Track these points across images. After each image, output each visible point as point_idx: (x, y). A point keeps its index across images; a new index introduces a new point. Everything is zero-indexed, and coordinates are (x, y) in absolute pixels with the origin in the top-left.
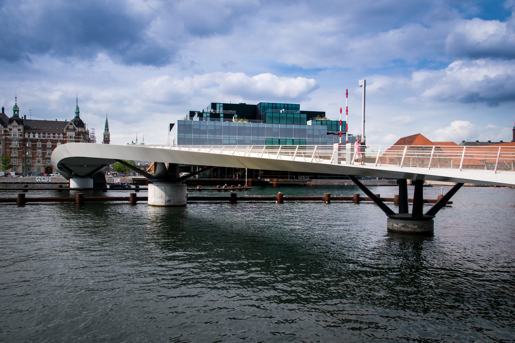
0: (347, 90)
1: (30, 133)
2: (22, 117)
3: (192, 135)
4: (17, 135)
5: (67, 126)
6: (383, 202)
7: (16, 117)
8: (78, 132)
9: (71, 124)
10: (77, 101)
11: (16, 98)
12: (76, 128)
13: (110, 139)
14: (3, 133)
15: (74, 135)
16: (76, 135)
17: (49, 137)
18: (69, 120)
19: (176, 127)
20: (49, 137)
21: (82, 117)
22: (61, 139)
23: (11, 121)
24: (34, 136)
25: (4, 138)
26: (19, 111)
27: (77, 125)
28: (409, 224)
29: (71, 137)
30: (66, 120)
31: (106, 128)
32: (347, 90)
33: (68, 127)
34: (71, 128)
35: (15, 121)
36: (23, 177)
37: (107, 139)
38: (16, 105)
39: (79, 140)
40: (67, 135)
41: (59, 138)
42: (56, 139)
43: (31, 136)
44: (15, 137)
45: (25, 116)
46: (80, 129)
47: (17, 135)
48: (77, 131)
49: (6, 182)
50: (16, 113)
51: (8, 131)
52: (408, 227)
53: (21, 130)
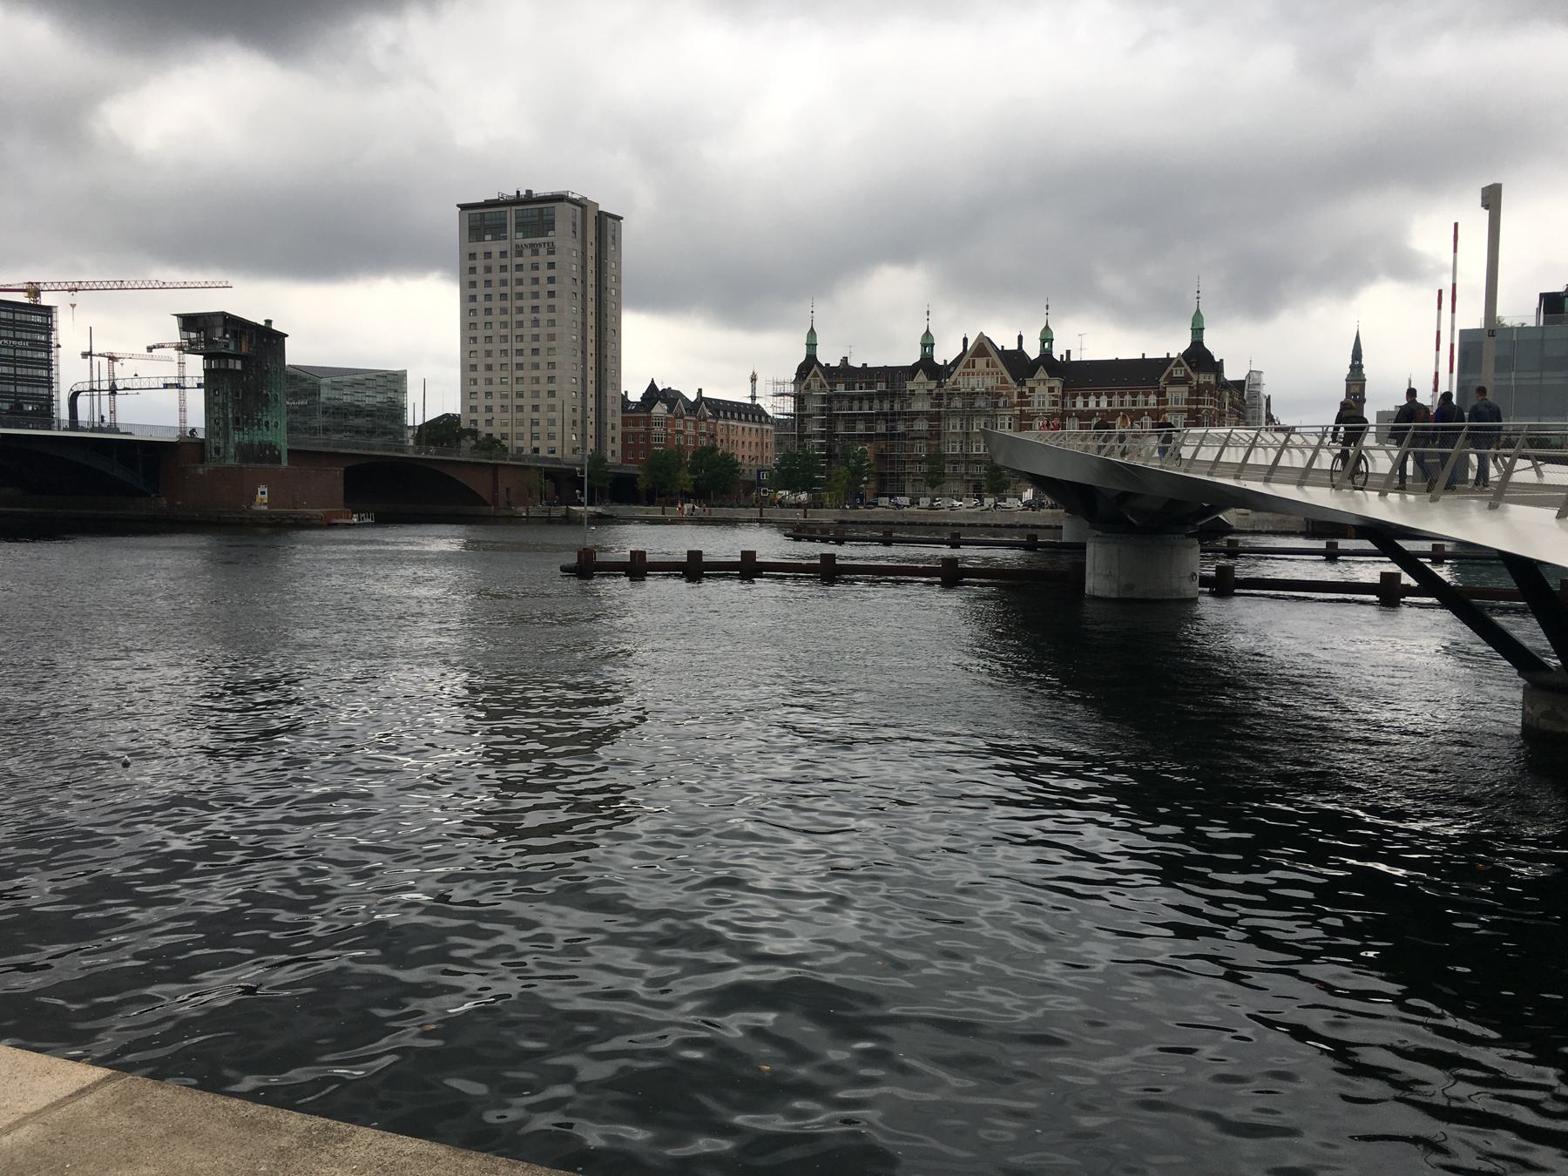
0: (1456, 225)
2: (1062, 356)
4: (1047, 403)
5: (1185, 365)
6: (1400, 543)
7: (1046, 355)
8: (1198, 385)
9: (1179, 364)
11: (928, 312)
12: (1192, 374)
13: (1366, 396)
14: (1015, 400)
15: (1186, 395)
16: (1191, 394)
17: (1134, 403)
18: (1173, 355)
20: (1122, 405)
22: (1152, 407)
23: (1035, 365)
24: (1086, 404)
25: (1018, 412)
26: (933, 344)
27: (1194, 365)
30: (1143, 355)
32: (1456, 225)
33: (1171, 372)
35: (1042, 367)
37: (1355, 396)
41: (1146, 404)
42: (1140, 407)
43: (1080, 405)
44: (1041, 407)
45: (1068, 352)
46: (1202, 375)
47: (1047, 403)
49: (989, 522)
53: (1056, 390)
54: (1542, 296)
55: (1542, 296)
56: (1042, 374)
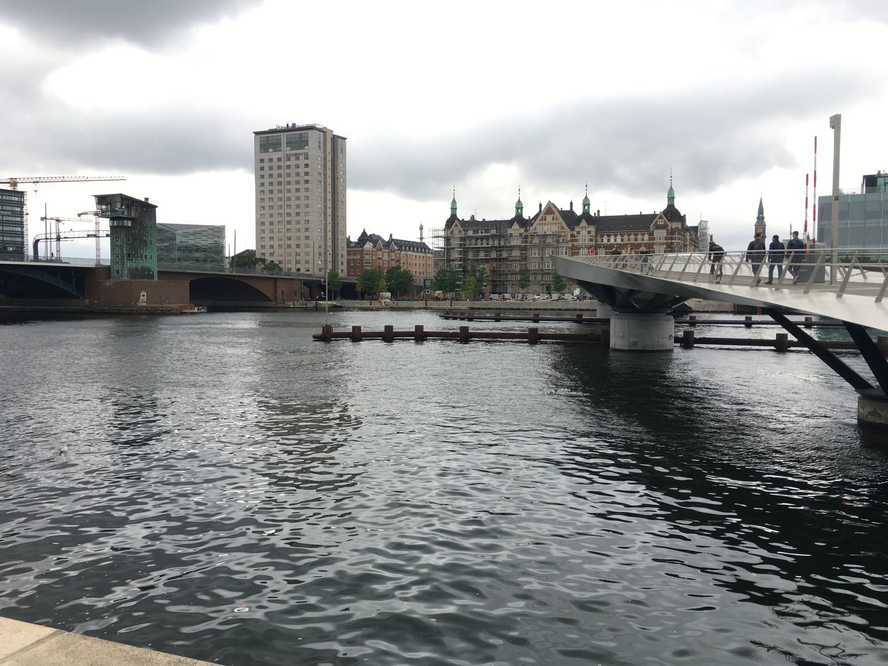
0: (816, 138)
1: (617, 235)
2: (595, 214)
3: (849, 223)
4: (587, 240)
7: (586, 214)
8: (672, 229)
9: (661, 217)
10: (671, 180)
11: (519, 190)
12: (668, 223)
14: (569, 238)
15: (665, 235)
18: (658, 212)
19: (263, 257)
21: (678, 205)
22: (646, 242)
24: (609, 240)
26: (589, 204)
27: (669, 218)
28: (882, 411)
29: (660, 239)
31: (759, 215)
34: (661, 223)
36: (580, 300)
38: (586, 197)
39: (673, 241)
40: (655, 235)
43: (605, 241)
44: (584, 242)
45: (599, 211)
46: (674, 224)
47: (587, 240)
48: (670, 228)
50: (586, 207)
51: (576, 235)
52: (880, 416)
53: (592, 232)
54: (865, 177)
55: (865, 177)
56: (584, 223)
